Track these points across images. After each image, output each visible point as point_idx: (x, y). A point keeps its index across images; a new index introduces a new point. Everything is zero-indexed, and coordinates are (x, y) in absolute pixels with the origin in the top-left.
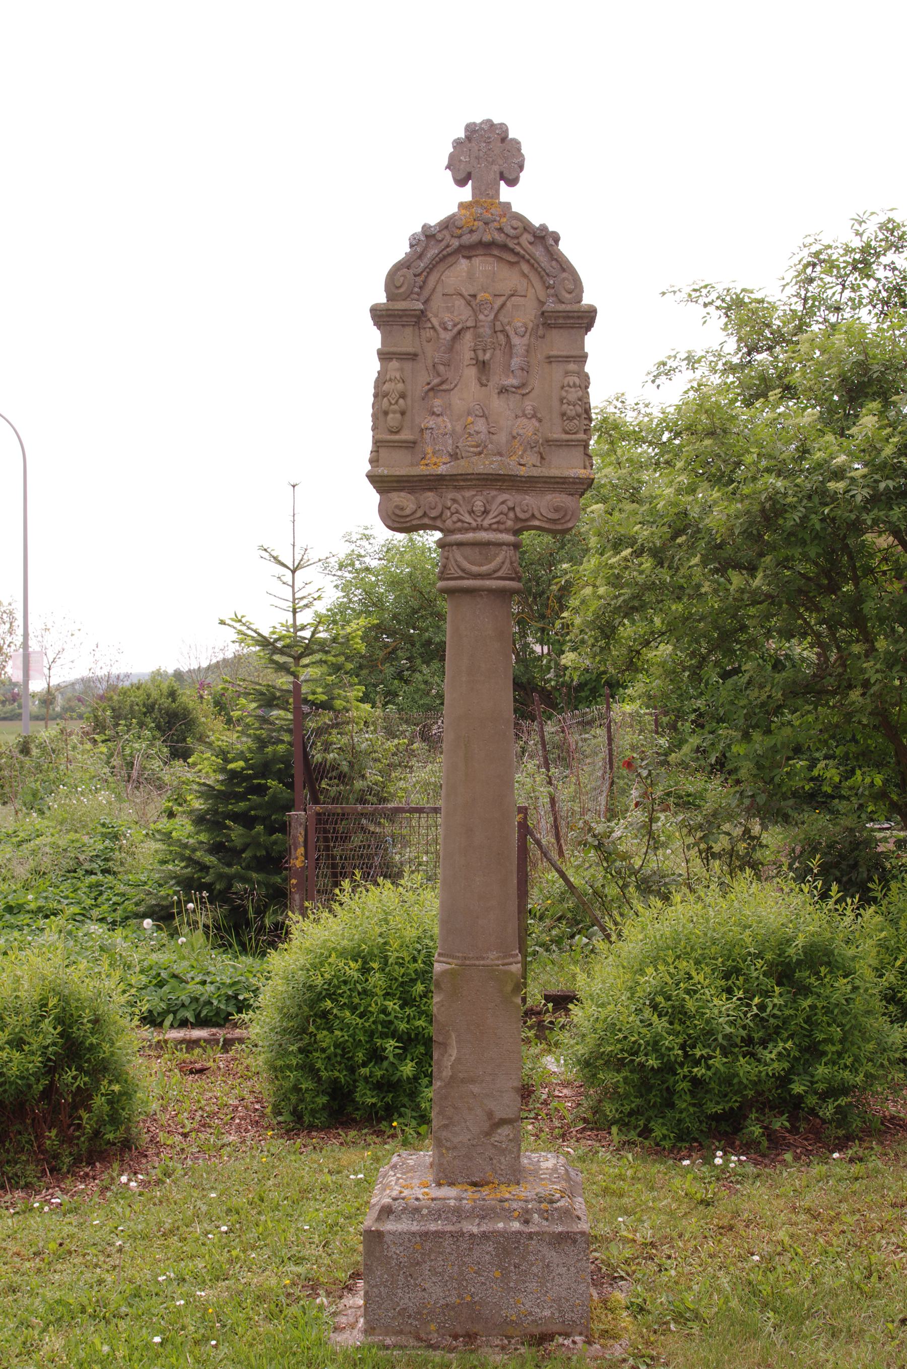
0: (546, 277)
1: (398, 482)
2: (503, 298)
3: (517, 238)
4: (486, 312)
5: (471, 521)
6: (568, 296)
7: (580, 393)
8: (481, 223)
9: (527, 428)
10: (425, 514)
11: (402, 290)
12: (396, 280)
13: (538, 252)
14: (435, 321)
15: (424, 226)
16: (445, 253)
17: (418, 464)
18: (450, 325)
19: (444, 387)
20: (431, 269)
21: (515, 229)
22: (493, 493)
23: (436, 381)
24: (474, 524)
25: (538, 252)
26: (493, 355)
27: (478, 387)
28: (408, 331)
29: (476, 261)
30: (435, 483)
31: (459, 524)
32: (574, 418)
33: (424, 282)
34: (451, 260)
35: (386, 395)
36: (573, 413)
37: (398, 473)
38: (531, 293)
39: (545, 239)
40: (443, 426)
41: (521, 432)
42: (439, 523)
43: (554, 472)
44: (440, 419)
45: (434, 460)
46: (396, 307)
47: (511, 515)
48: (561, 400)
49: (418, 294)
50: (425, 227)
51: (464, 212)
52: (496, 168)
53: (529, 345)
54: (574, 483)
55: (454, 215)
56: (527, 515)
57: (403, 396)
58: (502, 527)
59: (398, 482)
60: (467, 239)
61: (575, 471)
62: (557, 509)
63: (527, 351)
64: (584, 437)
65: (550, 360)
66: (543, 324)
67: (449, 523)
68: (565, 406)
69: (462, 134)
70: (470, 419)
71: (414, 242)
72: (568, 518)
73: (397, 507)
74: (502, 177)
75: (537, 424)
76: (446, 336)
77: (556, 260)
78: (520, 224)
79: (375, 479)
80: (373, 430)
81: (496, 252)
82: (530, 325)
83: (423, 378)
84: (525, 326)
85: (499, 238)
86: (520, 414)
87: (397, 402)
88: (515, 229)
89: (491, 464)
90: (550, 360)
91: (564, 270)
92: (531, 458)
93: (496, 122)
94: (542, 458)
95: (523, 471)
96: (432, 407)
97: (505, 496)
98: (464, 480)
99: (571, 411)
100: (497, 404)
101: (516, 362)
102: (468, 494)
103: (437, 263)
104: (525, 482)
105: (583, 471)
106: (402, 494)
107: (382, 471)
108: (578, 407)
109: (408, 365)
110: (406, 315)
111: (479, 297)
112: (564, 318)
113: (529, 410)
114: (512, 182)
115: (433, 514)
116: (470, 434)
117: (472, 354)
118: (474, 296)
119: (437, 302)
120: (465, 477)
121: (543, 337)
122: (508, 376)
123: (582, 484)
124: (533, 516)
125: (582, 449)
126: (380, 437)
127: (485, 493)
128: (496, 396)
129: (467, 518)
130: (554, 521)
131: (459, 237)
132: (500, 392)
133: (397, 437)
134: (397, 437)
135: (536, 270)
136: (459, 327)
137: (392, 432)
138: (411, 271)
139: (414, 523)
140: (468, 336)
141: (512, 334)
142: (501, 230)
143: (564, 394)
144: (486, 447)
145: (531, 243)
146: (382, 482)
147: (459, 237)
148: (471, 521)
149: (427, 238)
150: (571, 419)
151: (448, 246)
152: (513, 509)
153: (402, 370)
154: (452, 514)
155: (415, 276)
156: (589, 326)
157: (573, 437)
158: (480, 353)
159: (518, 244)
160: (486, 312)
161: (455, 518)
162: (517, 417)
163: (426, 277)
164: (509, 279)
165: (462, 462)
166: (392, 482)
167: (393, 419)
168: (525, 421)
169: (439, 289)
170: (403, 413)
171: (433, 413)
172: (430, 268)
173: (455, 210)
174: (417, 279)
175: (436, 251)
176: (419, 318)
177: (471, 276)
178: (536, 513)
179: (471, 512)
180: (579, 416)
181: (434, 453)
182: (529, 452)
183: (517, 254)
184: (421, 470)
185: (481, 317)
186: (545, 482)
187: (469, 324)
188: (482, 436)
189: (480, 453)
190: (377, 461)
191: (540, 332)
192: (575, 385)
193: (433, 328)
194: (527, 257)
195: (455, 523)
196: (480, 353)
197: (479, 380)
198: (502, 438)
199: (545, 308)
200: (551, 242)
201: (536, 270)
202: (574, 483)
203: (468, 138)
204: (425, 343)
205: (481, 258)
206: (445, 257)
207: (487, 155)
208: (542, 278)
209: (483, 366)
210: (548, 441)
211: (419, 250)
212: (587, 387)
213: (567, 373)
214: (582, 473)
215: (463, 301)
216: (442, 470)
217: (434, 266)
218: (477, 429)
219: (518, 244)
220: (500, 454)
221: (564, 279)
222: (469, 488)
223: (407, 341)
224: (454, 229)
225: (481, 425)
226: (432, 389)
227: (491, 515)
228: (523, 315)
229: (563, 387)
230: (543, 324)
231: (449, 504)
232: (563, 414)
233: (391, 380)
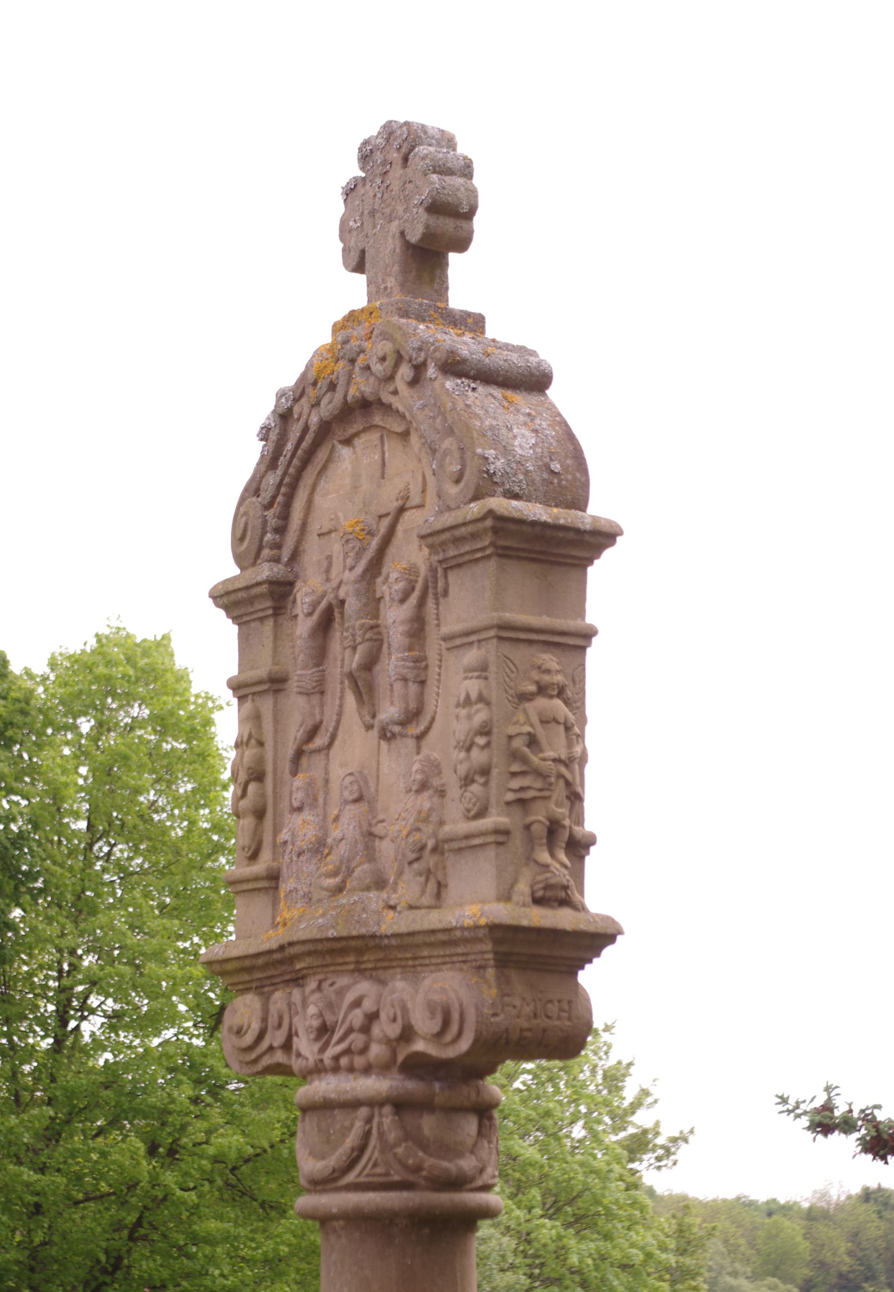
22: (343, 981)
34: (321, 455)
169: (315, 526)
174: (270, 514)
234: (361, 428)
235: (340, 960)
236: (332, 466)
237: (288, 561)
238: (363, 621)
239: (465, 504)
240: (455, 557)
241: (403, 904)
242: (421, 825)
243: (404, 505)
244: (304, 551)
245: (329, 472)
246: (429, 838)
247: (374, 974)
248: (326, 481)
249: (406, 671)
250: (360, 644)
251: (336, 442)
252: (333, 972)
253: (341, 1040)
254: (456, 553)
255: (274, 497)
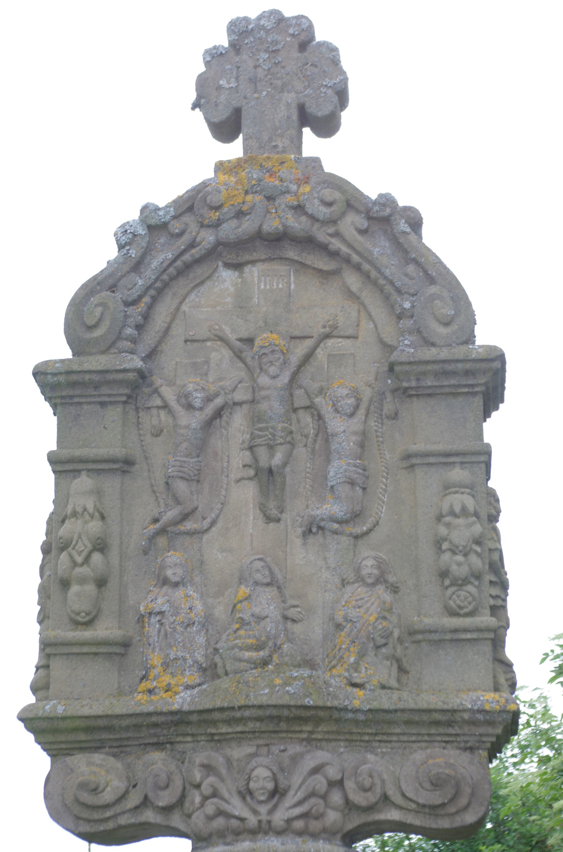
0: (395, 296)
1: (88, 730)
2: (309, 343)
3: (333, 222)
4: (273, 370)
5: (245, 813)
6: (443, 331)
7: (477, 529)
8: (258, 198)
9: (366, 606)
10: (146, 802)
11: (98, 333)
12: (92, 313)
13: (379, 249)
14: (169, 394)
15: (144, 209)
16: (187, 257)
17: (133, 691)
18: (198, 399)
19: (189, 525)
20: (160, 292)
21: (329, 204)
22: (295, 748)
23: (171, 514)
24: (252, 821)
25: (379, 249)
26: (289, 456)
27: (261, 522)
28: (114, 414)
29: (253, 273)
30: (167, 730)
31: (220, 822)
32: (465, 581)
33: (146, 317)
34: (200, 271)
35: (65, 546)
36: (464, 571)
37: (86, 711)
38: (366, 326)
39: (394, 223)
40: (185, 606)
41: (353, 613)
42: (176, 820)
43: (428, 700)
44: (180, 593)
45: (167, 679)
46: (86, 366)
47: (336, 797)
48: (438, 543)
49: (134, 341)
50: (148, 210)
51: (223, 178)
52: (290, 97)
53: (364, 434)
54: (473, 723)
55: (204, 184)
56: (371, 798)
57: (101, 546)
58: (315, 825)
59: (88, 730)
60: (230, 230)
61: (473, 695)
62: (437, 783)
63: (362, 445)
64: (491, 621)
65: (411, 461)
66: (394, 391)
67: (198, 819)
68: (446, 557)
69: (223, 40)
70: (244, 590)
71: (124, 239)
72: (463, 801)
73: (83, 786)
74: (305, 118)
75: (388, 597)
76: (194, 421)
77: (415, 261)
78: (337, 195)
79: (39, 725)
80: (40, 622)
81: (292, 254)
82: (367, 394)
83: (145, 509)
84: (356, 394)
85: (297, 224)
86: (351, 576)
87: (87, 560)
88: (329, 204)
89: (286, 684)
90: (411, 461)
91: (432, 280)
92: (376, 671)
93: (287, 14)
94: (402, 670)
95: (358, 699)
96: (162, 567)
97: (321, 756)
98: (228, 722)
99: (459, 566)
100: (302, 557)
101: (338, 469)
102: (238, 752)
103: (173, 278)
104: (366, 723)
105: (491, 696)
106: (97, 757)
107: (57, 708)
108: (473, 558)
109: (112, 485)
110: (108, 383)
111: (258, 342)
112: (437, 375)
113: (369, 567)
114: (327, 126)
115: (165, 799)
116: (243, 623)
117: (247, 456)
118: (250, 341)
119: (173, 358)
120: (231, 715)
121: (395, 416)
122: (322, 500)
123: (490, 723)
124: (385, 798)
125: (487, 648)
126: (52, 634)
127: (275, 749)
128: (299, 542)
129: (237, 807)
130: (434, 810)
131: (216, 225)
132: (308, 532)
133: (87, 634)
134: (87, 634)
135: (375, 283)
136: (219, 401)
137: (77, 624)
138: (118, 295)
139: (123, 820)
140: (238, 421)
141: (327, 410)
142: (299, 209)
143: (443, 531)
144: (277, 648)
145: (363, 232)
146: (55, 731)
147: (216, 225)
148: (245, 813)
149: (151, 231)
150: (460, 583)
151: (192, 245)
152: (340, 783)
153: (98, 493)
154: (205, 798)
155: (127, 304)
156: (492, 397)
157: (467, 622)
158: (262, 452)
159: (337, 235)
160: (273, 370)
161: (210, 809)
162: (344, 583)
163: (150, 307)
164: (318, 304)
165: (225, 683)
166: (75, 730)
167: (80, 596)
168: (361, 591)
169: (179, 331)
170: (101, 583)
171: (165, 582)
172: (159, 290)
173: (210, 174)
174: (130, 310)
175: (169, 251)
176: (135, 386)
177: (242, 303)
178: (391, 792)
179: (246, 794)
180: (478, 577)
181: (166, 665)
182: (371, 657)
183: (334, 254)
184: (140, 702)
185: (264, 380)
186: (408, 723)
187: (238, 396)
188: (269, 626)
189: (265, 663)
190: (46, 687)
191: (388, 407)
192: (464, 512)
193: (165, 406)
194: (355, 258)
195: (210, 818)
196: (262, 452)
197: (263, 508)
198: (314, 629)
199: (395, 356)
200: (403, 226)
201: (375, 283)
202: (473, 723)
203: (235, 46)
204: (148, 438)
205: (260, 266)
206: (188, 266)
207: (272, 83)
208: (387, 298)
209: (268, 479)
210: (412, 633)
211: (133, 253)
212: (494, 518)
213: (448, 488)
214: (490, 700)
215: (226, 353)
216: (182, 700)
217: (166, 285)
218: (257, 610)
219: (337, 235)
220: (311, 665)
221: (433, 297)
222: (240, 738)
223: (109, 434)
224: (205, 211)
225: (266, 603)
226: (163, 531)
227: (290, 800)
228: (352, 371)
229: (439, 518)
230: (394, 391)
231: (198, 776)
232: (444, 574)
233: (74, 514)
234: (264, 257)
235: (297, 728)
236: (209, 283)
237: (145, 357)
238: (286, 425)
239: (458, 344)
240: (430, 387)
241: (375, 681)
242: (387, 615)
243: (331, 333)
244: (162, 352)
245: (203, 288)
246: (395, 627)
247: (318, 744)
248: (196, 295)
249: (356, 476)
250: (281, 444)
251: (220, 263)
252: (380, 741)
253: (300, 803)
254: (435, 384)
255: (140, 297)
